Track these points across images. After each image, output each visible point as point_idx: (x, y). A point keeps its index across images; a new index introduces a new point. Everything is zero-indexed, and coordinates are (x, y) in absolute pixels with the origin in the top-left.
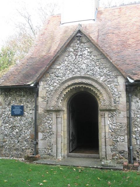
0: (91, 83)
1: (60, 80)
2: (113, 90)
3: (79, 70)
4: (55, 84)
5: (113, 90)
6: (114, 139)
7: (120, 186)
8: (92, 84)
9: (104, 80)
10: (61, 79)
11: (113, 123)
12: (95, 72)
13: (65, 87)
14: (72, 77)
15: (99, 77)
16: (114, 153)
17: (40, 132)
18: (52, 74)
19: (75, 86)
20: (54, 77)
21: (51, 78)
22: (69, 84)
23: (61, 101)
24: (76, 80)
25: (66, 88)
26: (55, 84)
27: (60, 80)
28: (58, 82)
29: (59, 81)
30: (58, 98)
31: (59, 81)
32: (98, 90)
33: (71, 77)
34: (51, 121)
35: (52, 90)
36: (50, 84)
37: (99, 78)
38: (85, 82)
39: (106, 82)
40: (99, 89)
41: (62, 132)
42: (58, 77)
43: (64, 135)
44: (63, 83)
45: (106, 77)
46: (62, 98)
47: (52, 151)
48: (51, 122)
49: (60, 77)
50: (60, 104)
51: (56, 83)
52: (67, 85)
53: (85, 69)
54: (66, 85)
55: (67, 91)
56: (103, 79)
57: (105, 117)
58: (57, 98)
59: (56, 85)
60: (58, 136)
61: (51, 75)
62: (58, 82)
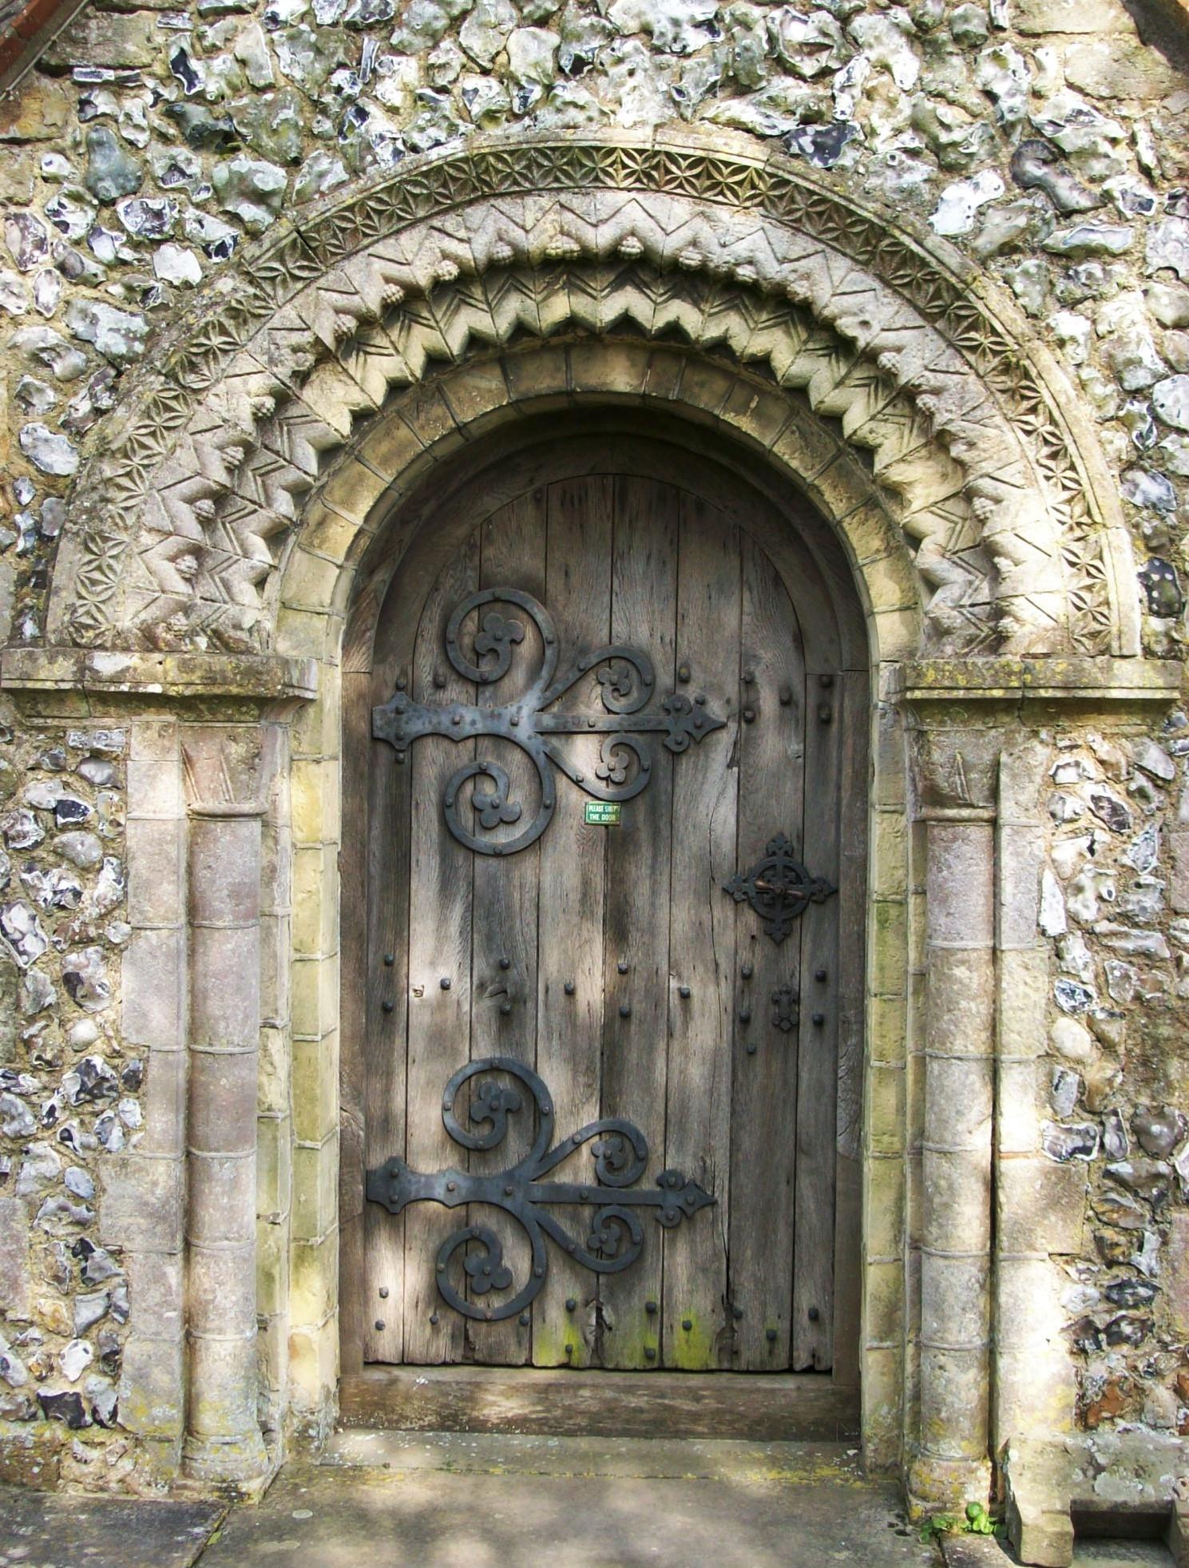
0: (774, 271)
1: (260, 197)
2: (1136, 394)
3: (577, 49)
4: (178, 264)
5: (1136, 394)
6: (1124, 1168)
7: (1186, 763)
8: (800, 289)
9: (999, 227)
10: (270, 177)
11: (1126, 918)
12: (844, 103)
13: (349, 323)
14: (477, 161)
15: (908, 179)
16: (1112, 1363)
17: (1179, 431)
18: (118, 88)
19: (513, 307)
20: (158, 158)
21: (100, 164)
22: (404, 273)
23: (262, 555)
24: (531, 209)
25: (353, 343)
26: (178, 264)
27: (260, 197)
28: (218, 230)
29: (235, 218)
30: (220, 497)
31: (235, 218)
32: (904, 397)
33: (455, 148)
34: (89, 870)
35: (115, 362)
36: (92, 267)
37: (910, 193)
38: (692, 258)
39: (1030, 263)
40: (909, 369)
41: (278, 1044)
42: (224, 142)
43: (302, 1093)
44: (313, 250)
45: (1028, 185)
46: (284, 505)
47: (109, 1361)
48: (105, 885)
49: (258, 152)
50: (246, 592)
51: (180, 238)
52: (373, 295)
53: (696, 39)
54: (369, 280)
55: (374, 375)
56: (981, 213)
57: (994, 823)
58: (209, 494)
59: (196, 276)
60: (216, 1125)
61: (103, 102)
62: (218, 230)
